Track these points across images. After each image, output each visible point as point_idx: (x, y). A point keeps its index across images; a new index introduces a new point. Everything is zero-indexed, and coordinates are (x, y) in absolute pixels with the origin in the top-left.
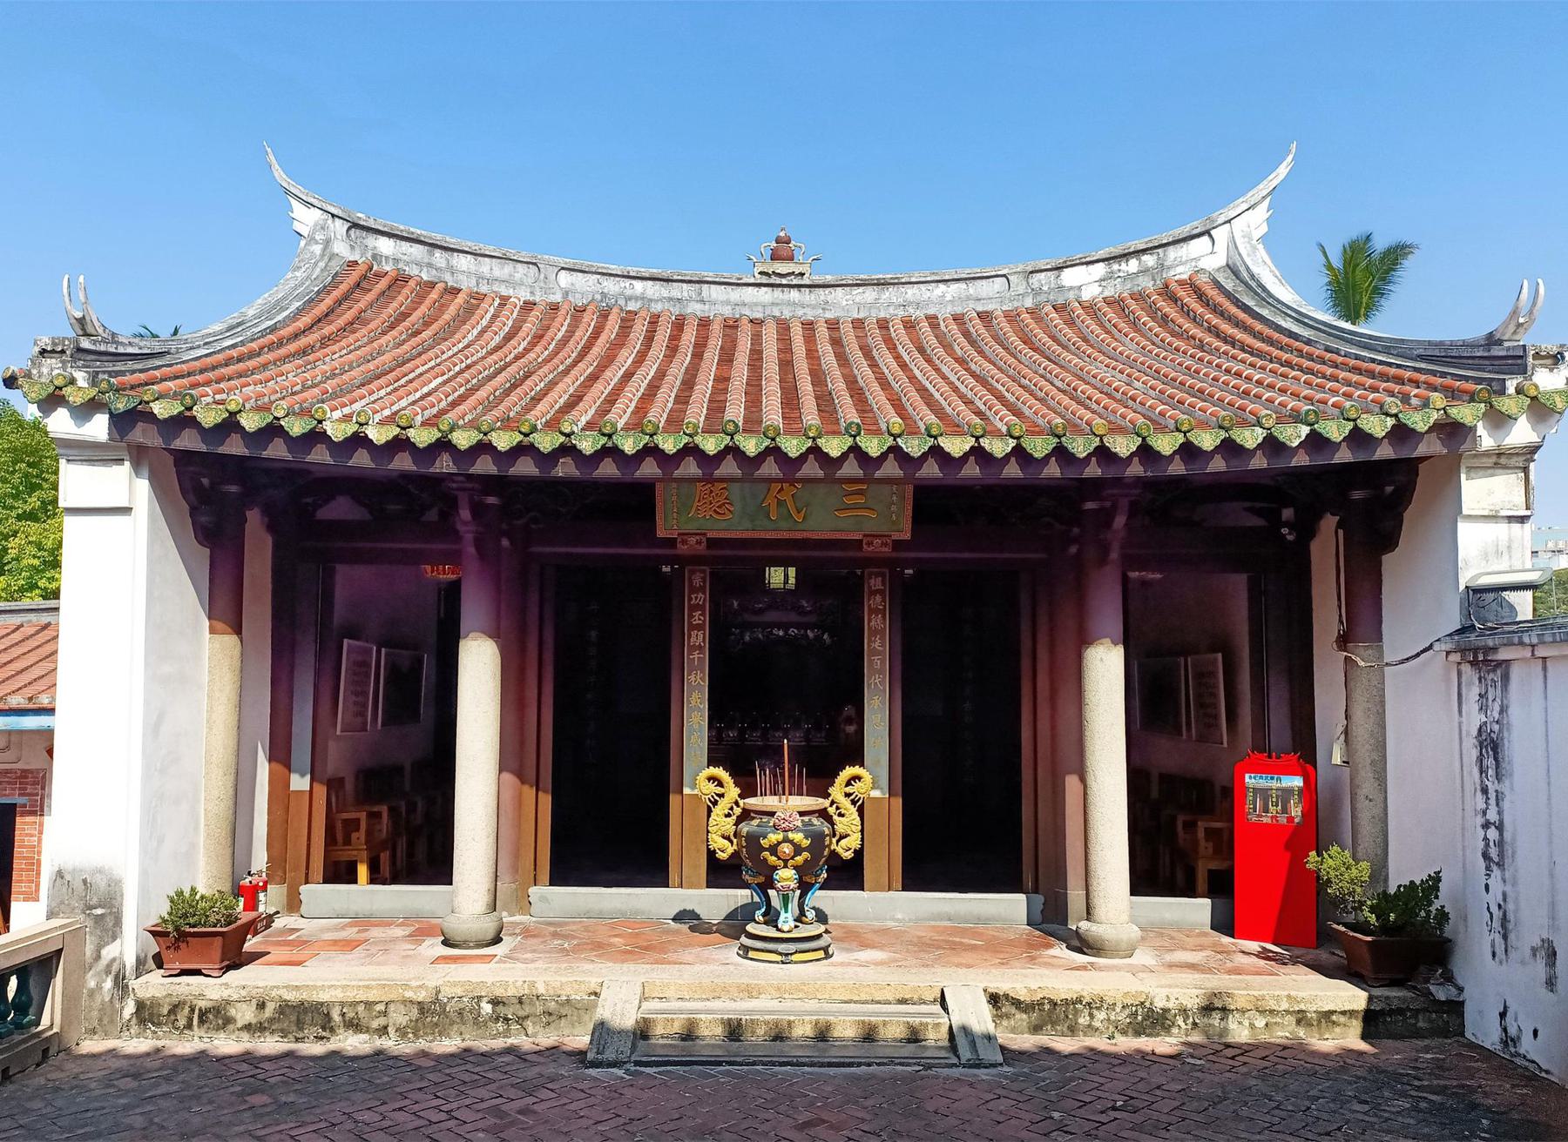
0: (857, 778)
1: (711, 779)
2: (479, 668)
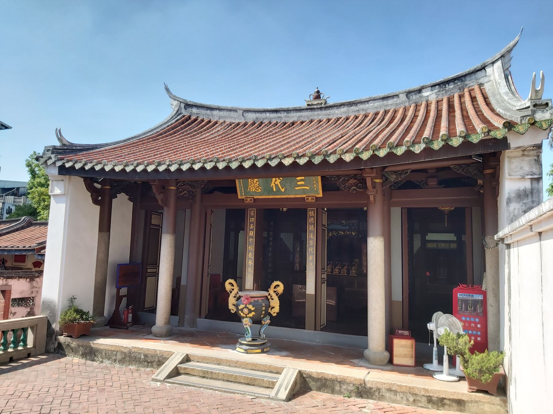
0: (278, 286)
1: (230, 283)
2: (375, 247)
